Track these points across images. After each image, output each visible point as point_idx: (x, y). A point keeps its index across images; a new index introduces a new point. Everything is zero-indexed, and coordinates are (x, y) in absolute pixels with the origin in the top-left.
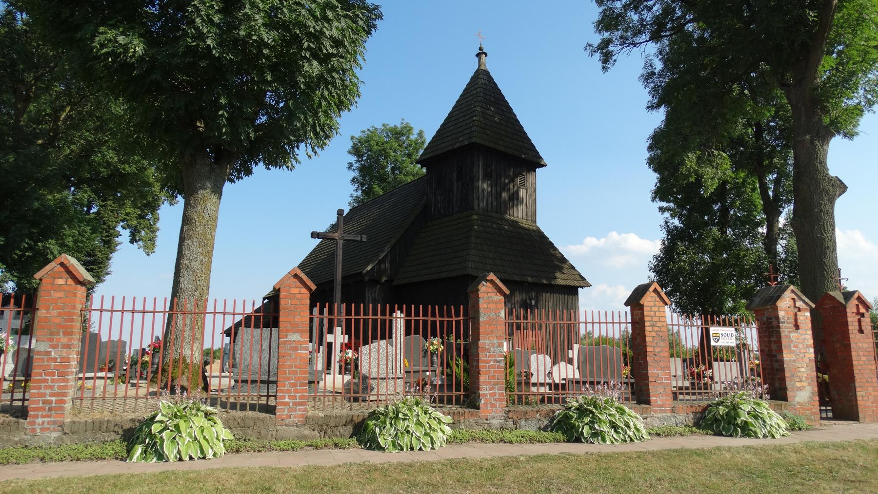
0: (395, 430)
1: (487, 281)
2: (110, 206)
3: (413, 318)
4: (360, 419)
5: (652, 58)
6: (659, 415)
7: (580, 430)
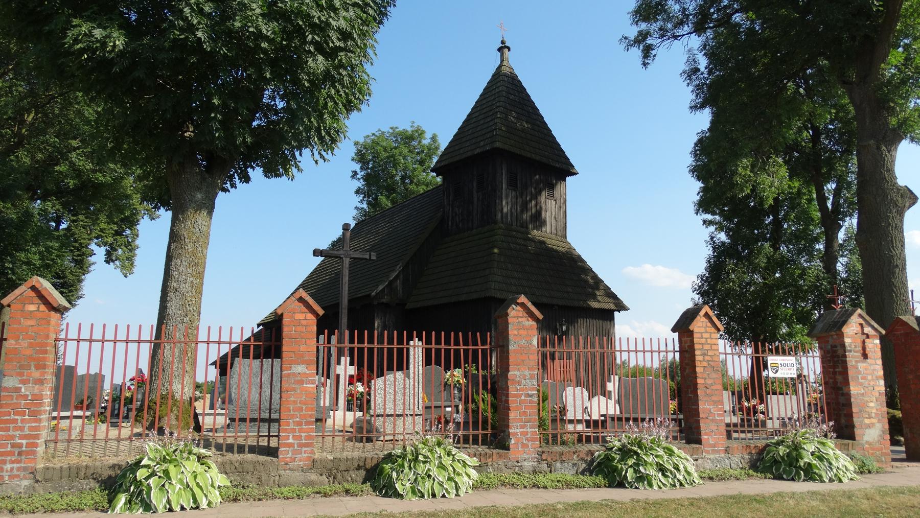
0: (414, 474)
1: (517, 304)
2: (82, 221)
3: (433, 346)
4: (375, 462)
5: (696, 52)
6: (712, 456)
7: (623, 473)
